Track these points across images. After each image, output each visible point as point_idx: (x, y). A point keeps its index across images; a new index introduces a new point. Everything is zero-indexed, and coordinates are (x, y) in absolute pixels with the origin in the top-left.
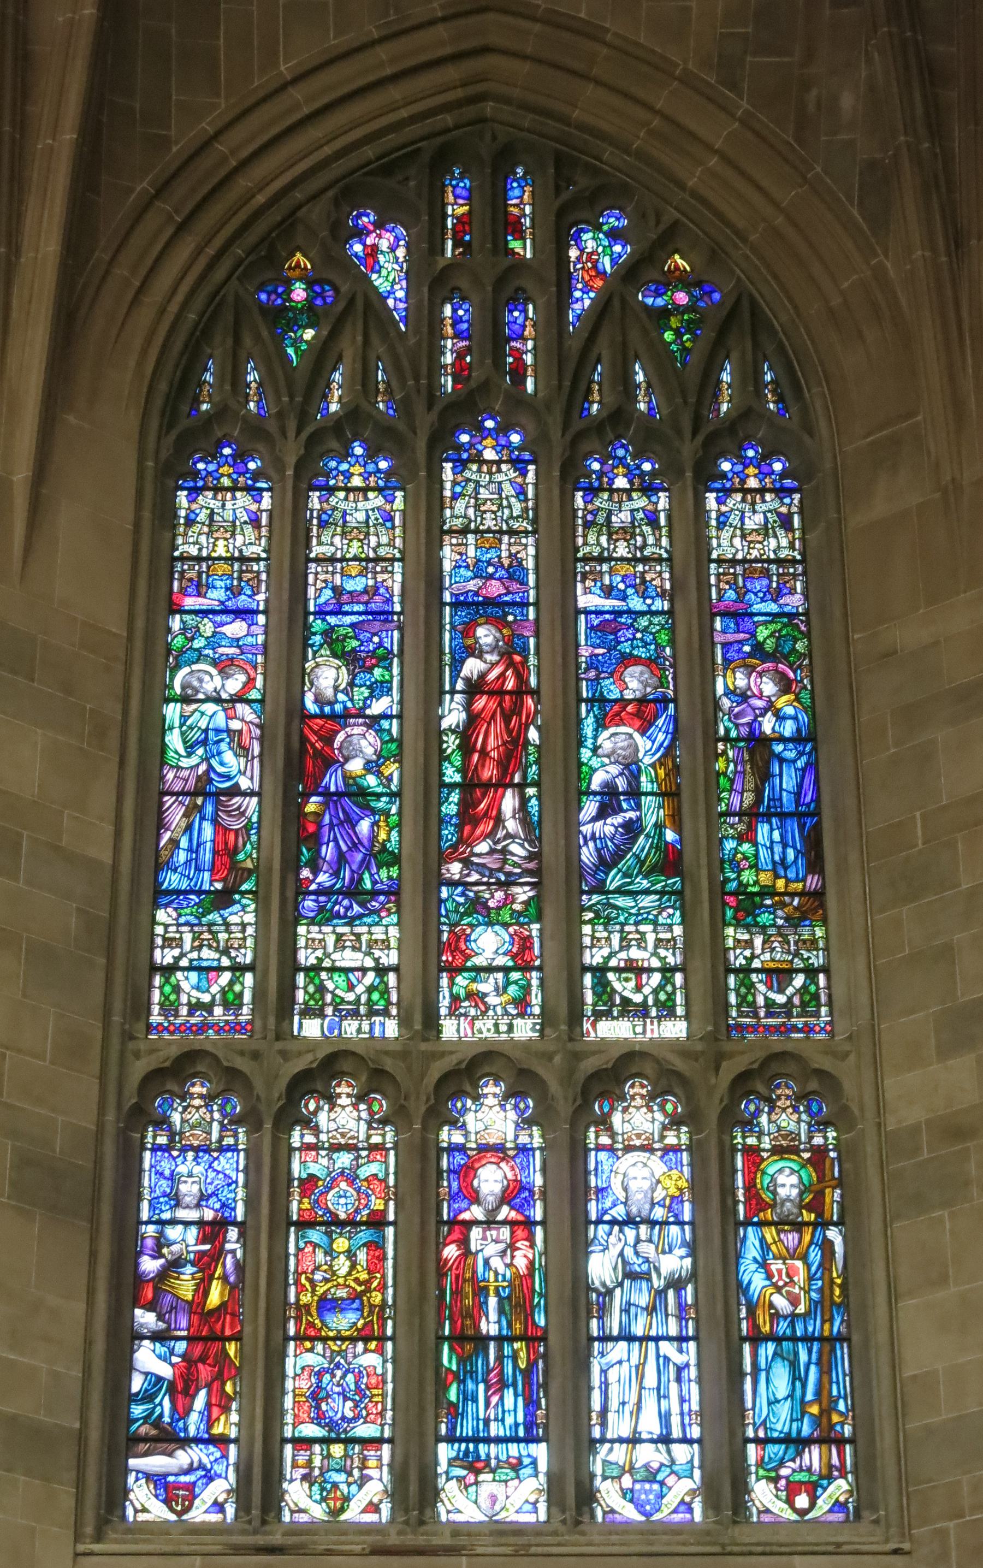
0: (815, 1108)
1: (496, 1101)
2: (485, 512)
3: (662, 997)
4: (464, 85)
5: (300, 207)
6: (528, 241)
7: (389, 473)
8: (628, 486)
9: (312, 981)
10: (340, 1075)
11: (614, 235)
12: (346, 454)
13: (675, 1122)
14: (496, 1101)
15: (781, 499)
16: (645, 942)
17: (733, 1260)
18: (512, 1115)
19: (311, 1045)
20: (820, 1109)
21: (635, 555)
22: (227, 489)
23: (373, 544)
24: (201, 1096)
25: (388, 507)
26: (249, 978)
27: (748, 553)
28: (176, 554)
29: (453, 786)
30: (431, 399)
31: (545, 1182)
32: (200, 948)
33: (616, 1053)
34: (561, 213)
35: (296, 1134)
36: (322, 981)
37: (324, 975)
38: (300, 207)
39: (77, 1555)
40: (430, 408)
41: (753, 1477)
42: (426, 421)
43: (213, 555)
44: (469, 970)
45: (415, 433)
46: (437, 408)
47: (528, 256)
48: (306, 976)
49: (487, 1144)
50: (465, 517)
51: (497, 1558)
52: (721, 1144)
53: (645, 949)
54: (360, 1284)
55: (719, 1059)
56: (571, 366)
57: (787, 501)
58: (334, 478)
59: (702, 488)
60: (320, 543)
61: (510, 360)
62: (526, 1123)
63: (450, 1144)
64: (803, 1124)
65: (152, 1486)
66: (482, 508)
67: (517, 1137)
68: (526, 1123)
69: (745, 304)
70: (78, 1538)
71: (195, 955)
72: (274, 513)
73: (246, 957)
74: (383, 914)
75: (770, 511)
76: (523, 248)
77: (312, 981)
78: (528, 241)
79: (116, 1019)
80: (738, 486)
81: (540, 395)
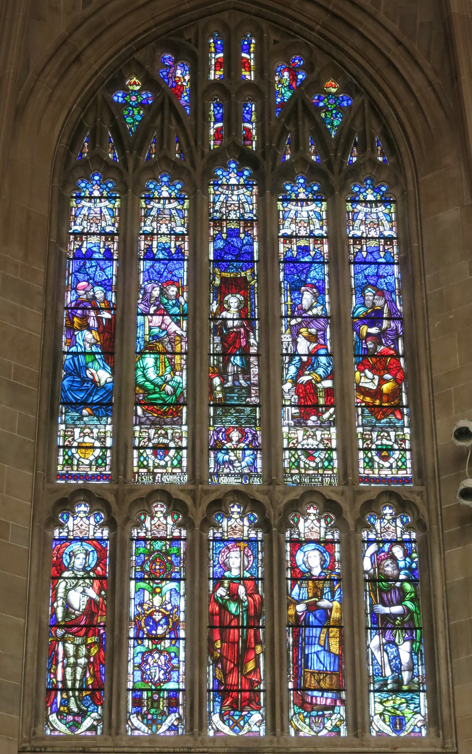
0: (405, 520)
1: (238, 516)
2: (231, 210)
3: (400, 464)
6: (252, 72)
9: (293, 456)
12: (89, 179)
14: (238, 516)
16: (316, 436)
18: (323, 524)
20: (408, 520)
22: (97, 197)
24: (238, 513)
26: (184, 452)
27: (90, 230)
28: (71, 231)
29: (253, 355)
36: (372, 456)
37: (74, 450)
42: (200, 164)
43: (369, 236)
44: (224, 449)
47: (252, 79)
48: (64, 451)
49: (310, 539)
50: (220, 212)
53: (167, 438)
54: (167, 611)
57: (389, 207)
58: (84, 192)
59: (137, 198)
60: (75, 225)
62: (179, 525)
63: (368, 539)
64: (322, 529)
65: (140, 717)
66: (230, 208)
68: (407, 528)
69: (167, 102)
71: (81, 440)
75: (311, 211)
77: (293, 456)
78: (252, 72)
80: (88, 195)
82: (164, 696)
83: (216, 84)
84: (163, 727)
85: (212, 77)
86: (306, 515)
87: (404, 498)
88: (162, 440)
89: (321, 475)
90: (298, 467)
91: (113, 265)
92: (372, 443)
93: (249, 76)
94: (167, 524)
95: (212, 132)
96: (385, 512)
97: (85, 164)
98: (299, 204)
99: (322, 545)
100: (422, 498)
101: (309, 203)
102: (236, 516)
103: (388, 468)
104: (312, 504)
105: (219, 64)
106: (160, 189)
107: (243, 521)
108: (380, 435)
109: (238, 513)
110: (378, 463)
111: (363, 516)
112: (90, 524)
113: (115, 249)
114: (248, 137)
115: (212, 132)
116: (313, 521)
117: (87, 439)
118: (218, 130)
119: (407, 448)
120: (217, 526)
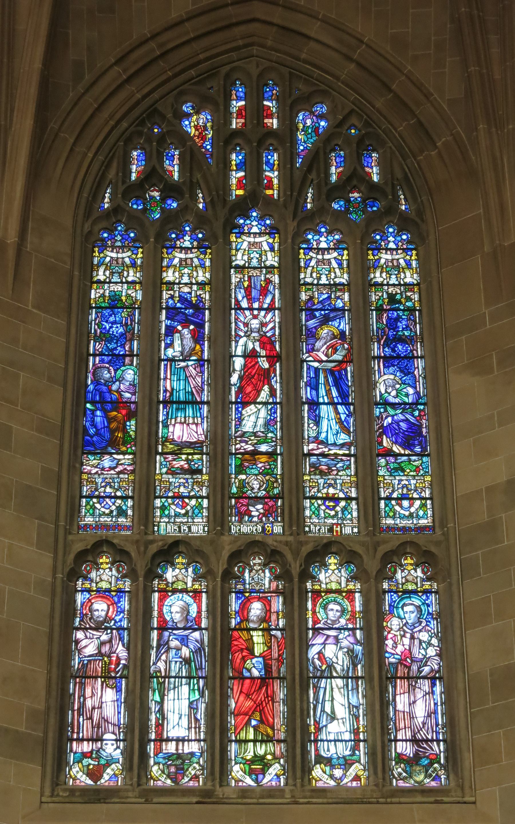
4: (242, 38)
5: (157, 101)
7: (409, 242)
8: (190, 246)
10: (405, 554)
11: (321, 117)
13: (353, 578)
15: (406, 253)
17: (305, 649)
19: (164, 538)
21: (400, 282)
23: (332, 277)
25: (340, 258)
30: (225, 201)
31: (130, 607)
32: (105, 487)
33: (171, 541)
34: (292, 106)
35: (80, 583)
38: (157, 101)
39: (42, 802)
40: (224, 207)
41: (233, 762)
42: (222, 213)
45: (217, 220)
46: (228, 207)
51: (239, 806)
52: (300, 588)
55: (376, 545)
56: (297, 185)
61: (266, 181)
62: (353, 578)
67: (193, 585)
70: (42, 795)
72: (350, 261)
73: (427, 494)
74: (263, 468)
76: (275, 123)
79: (62, 523)
81: (281, 200)
82: (439, 746)
83: (236, 133)
84: (267, 776)
85: (234, 126)
86: (324, 565)
87: (166, 547)
88: (331, 491)
89: (340, 525)
90: (318, 516)
91: (345, 317)
92: (319, 491)
93: (275, 123)
94: (341, 576)
95: (234, 181)
96: (330, 561)
97: (311, 216)
98: (183, 251)
99: (191, 594)
100: (138, 548)
101: (330, 251)
102: (333, 567)
103: (408, 517)
104: (256, 554)
105: (239, 114)
106: (183, 238)
107: (340, 572)
108: (326, 483)
109: (259, 564)
110: (399, 513)
111: (308, 566)
112: (112, 575)
113: (416, 299)
114: (270, 186)
115: (234, 181)
116: (333, 571)
117: (331, 491)
118: (240, 180)
119: (427, 496)
120: (314, 578)
